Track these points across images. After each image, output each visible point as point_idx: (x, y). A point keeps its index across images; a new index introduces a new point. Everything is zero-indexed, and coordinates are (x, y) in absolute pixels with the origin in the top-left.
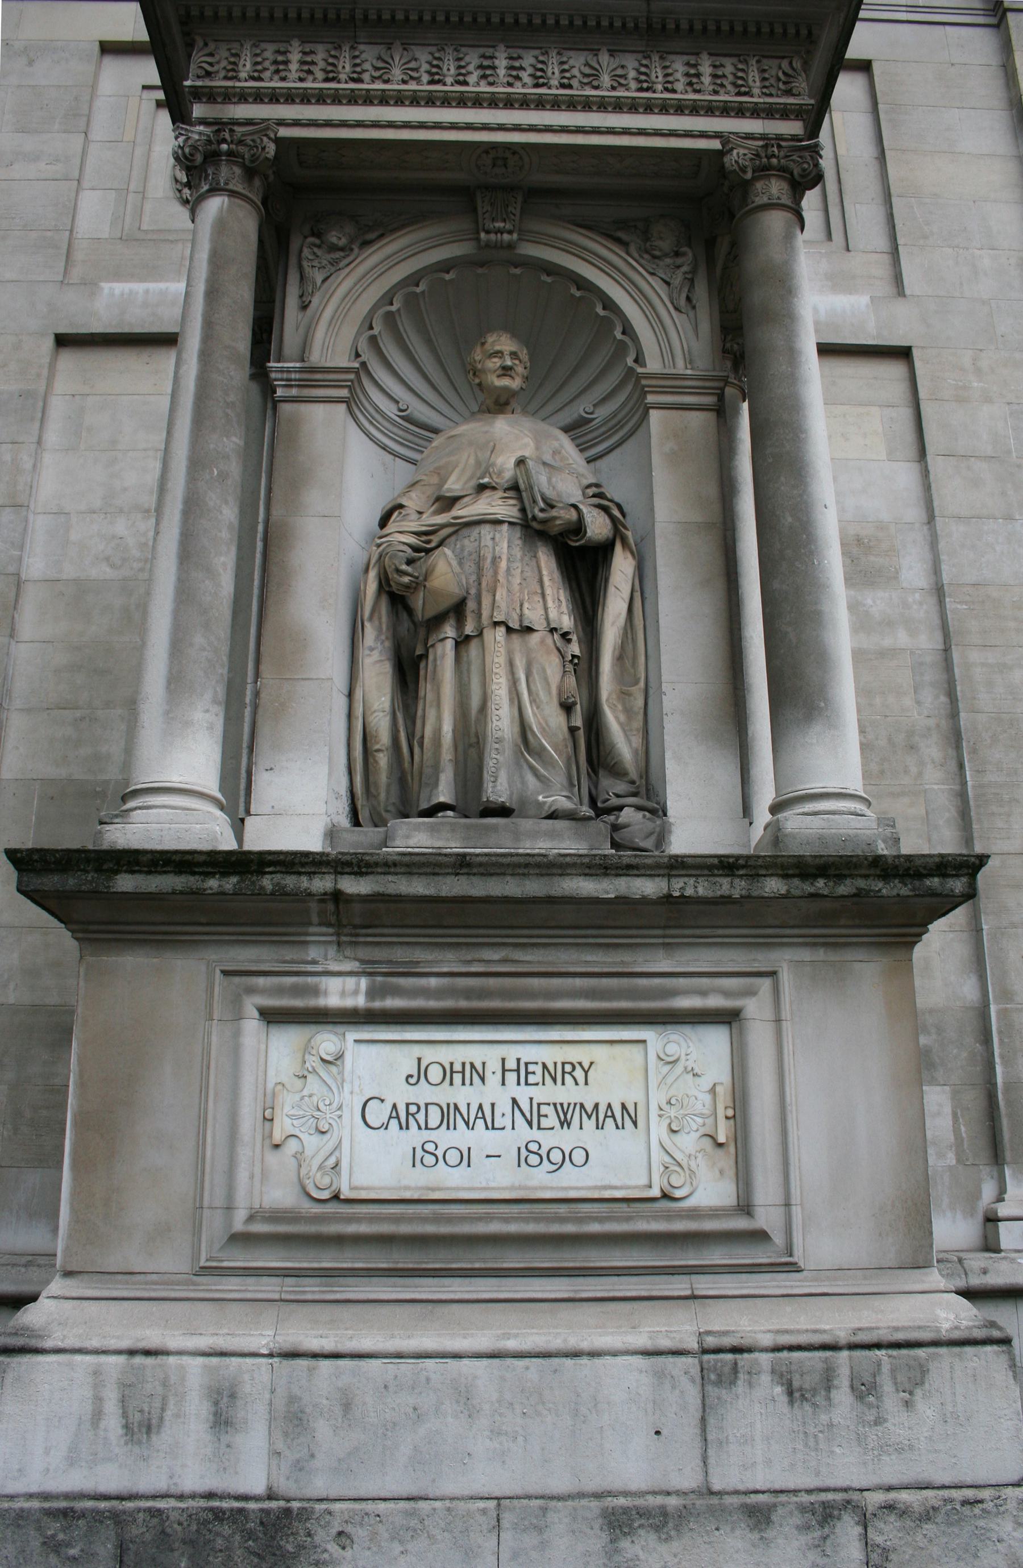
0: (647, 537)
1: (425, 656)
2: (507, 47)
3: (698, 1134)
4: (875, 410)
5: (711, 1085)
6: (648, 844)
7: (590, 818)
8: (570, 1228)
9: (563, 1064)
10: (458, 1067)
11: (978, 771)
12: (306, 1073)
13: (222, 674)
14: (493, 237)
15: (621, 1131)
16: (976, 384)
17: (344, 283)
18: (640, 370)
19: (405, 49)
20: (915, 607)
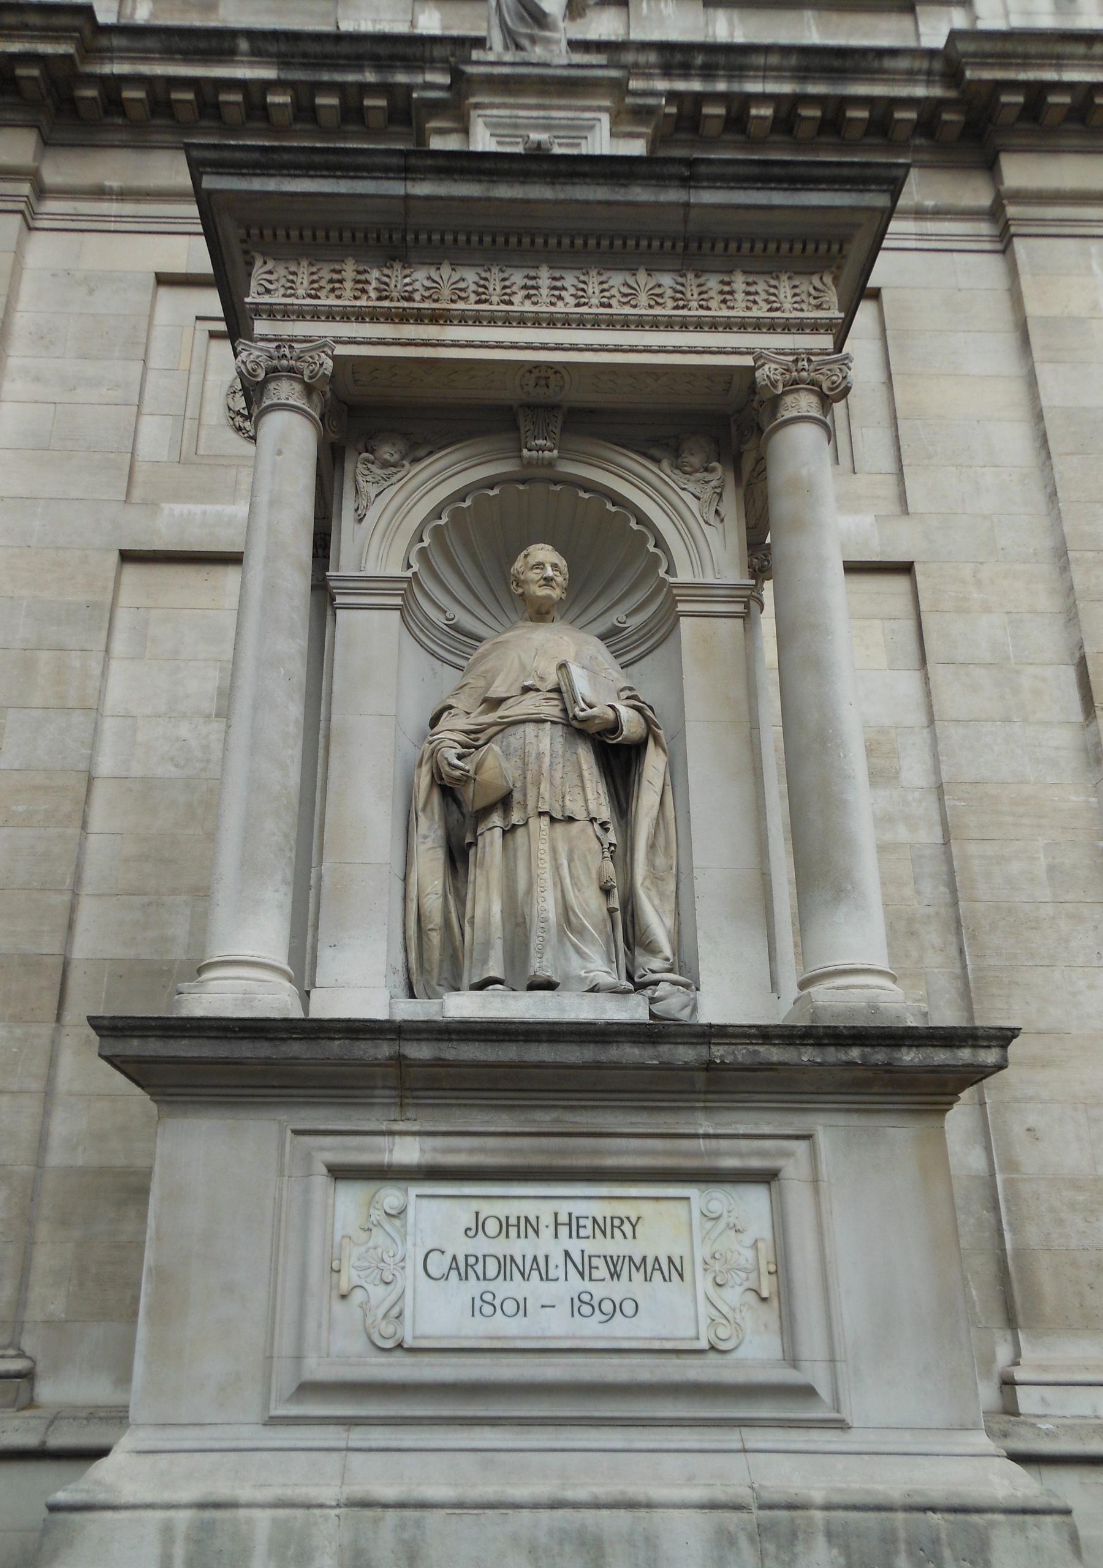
0: (679, 734)
1: (474, 844)
2: (551, 268)
4: (877, 623)
5: (752, 1242)
9: (612, 1218)
10: (513, 1221)
11: (978, 956)
12: (371, 1226)
13: (290, 858)
14: (534, 453)
15: (668, 1284)
16: (976, 595)
18: (672, 580)
19: (453, 269)
20: (914, 804)
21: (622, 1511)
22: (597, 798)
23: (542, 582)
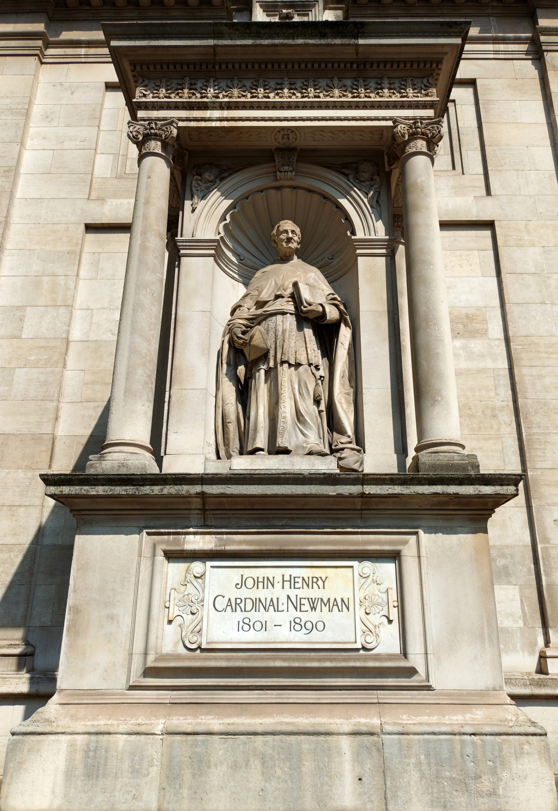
2: (289, 78)
6: (356, 467)
7: (327, 455)
9: (312, 578)
10: (261, 579)
11: (528, 428)
12: (186, 583)
13: (151, 388)
15: (341, 613)
19: (239, 81)
20: (495, 348)
21: (311, 736)
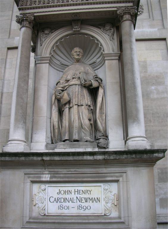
1: (64, 111)
3: (111, 203)
4: (159, 51)
8: (87, 221)
10: (66, 191)
14: (75, 29)
15: (97, 203)
17: (48, 40)
22: (87, 99)
23: (77, 55)
